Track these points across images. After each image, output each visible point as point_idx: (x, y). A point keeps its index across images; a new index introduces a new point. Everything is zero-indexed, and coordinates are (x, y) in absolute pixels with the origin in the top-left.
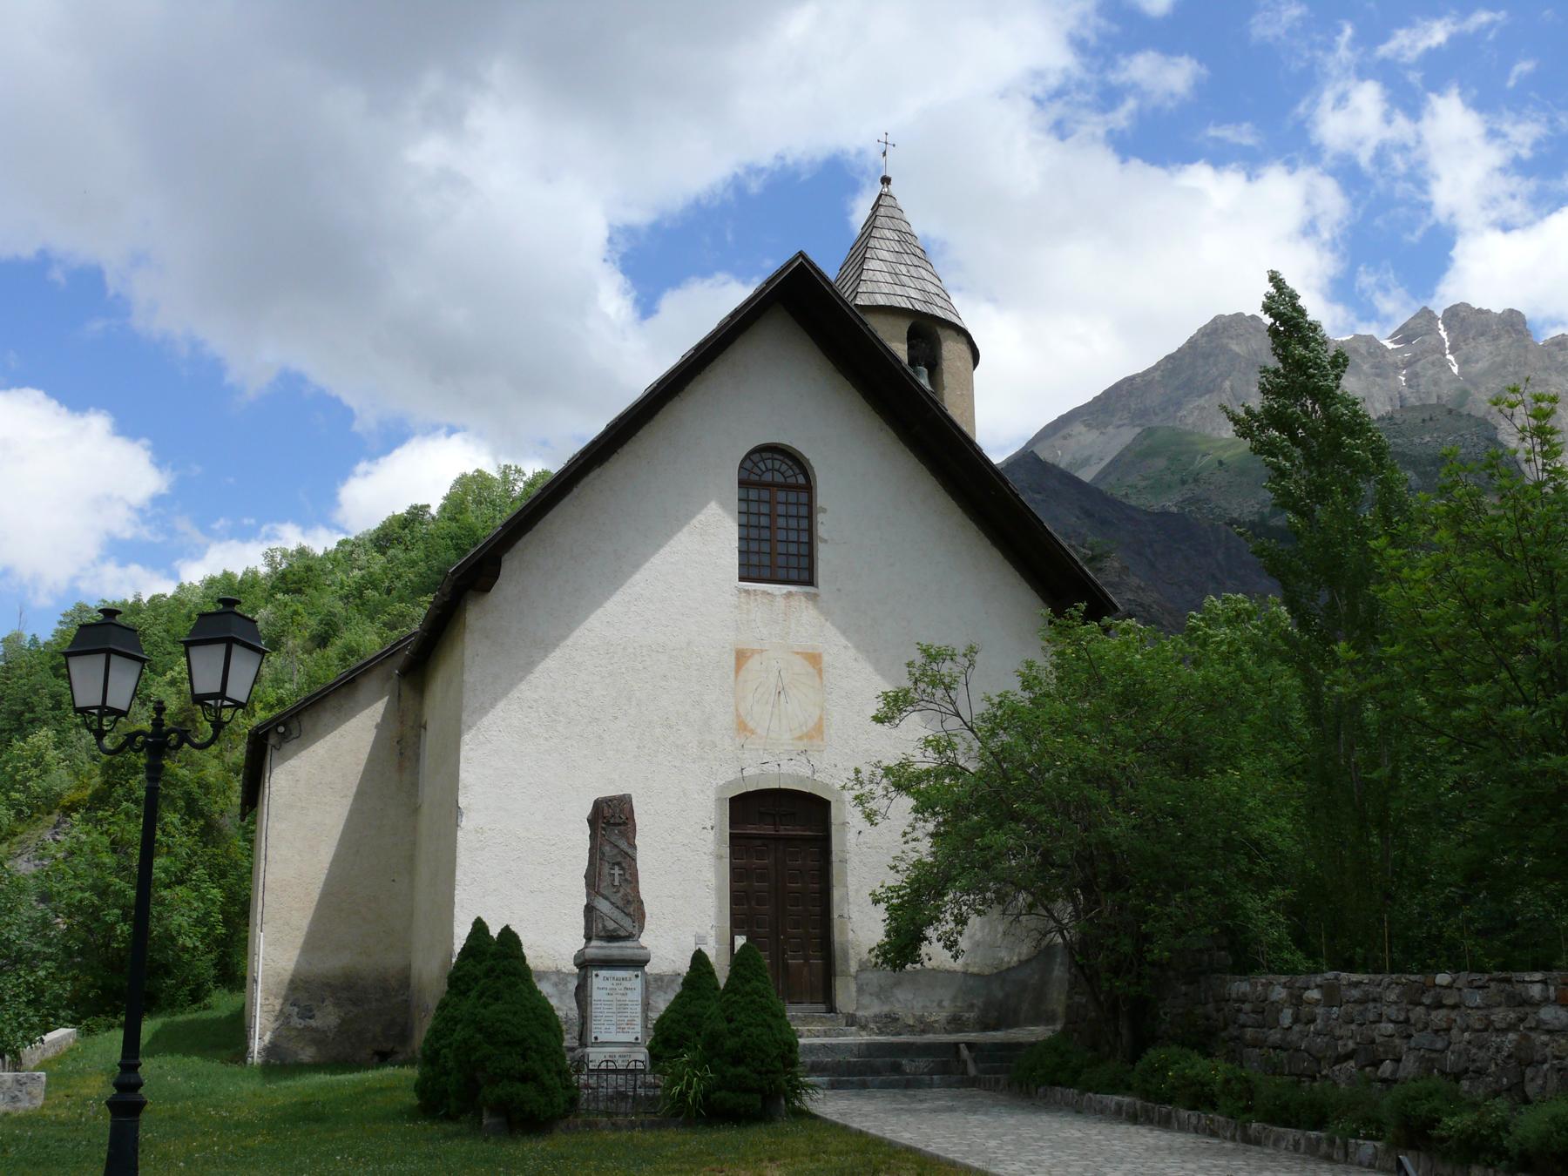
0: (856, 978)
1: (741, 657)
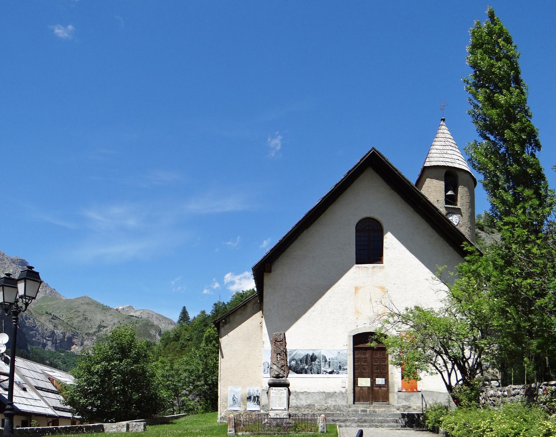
1: (357, 289)
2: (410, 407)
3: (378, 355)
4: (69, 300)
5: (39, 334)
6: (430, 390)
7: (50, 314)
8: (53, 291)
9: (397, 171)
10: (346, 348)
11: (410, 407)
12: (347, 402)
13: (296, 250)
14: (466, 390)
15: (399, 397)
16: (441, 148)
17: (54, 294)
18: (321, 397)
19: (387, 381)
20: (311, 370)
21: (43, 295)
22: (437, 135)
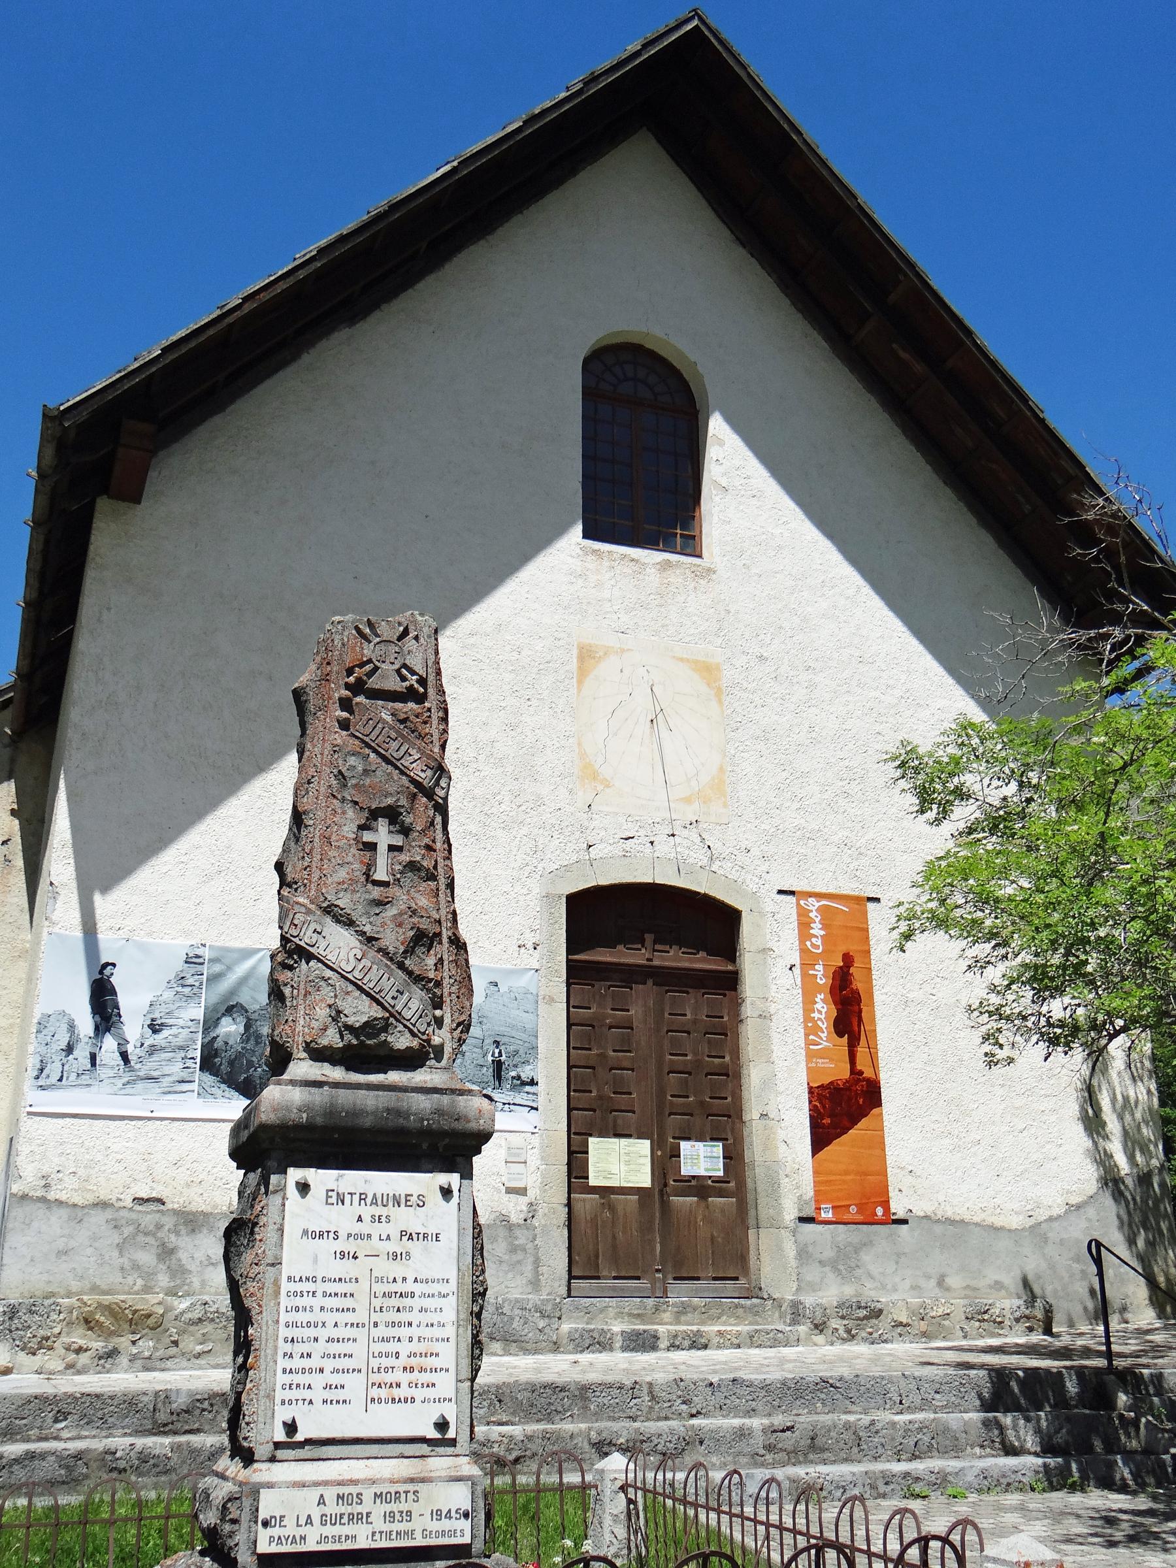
0: (794, 1232)
1: (587, 656)
2: (877, 1314)
3: (693, 1007)
9: (799, 133)
10: (533, 960)
11: (877, 1314)
12: (535, 1284)
13: (287, 413)
15: (803, 1254)
19: (734, 1158)
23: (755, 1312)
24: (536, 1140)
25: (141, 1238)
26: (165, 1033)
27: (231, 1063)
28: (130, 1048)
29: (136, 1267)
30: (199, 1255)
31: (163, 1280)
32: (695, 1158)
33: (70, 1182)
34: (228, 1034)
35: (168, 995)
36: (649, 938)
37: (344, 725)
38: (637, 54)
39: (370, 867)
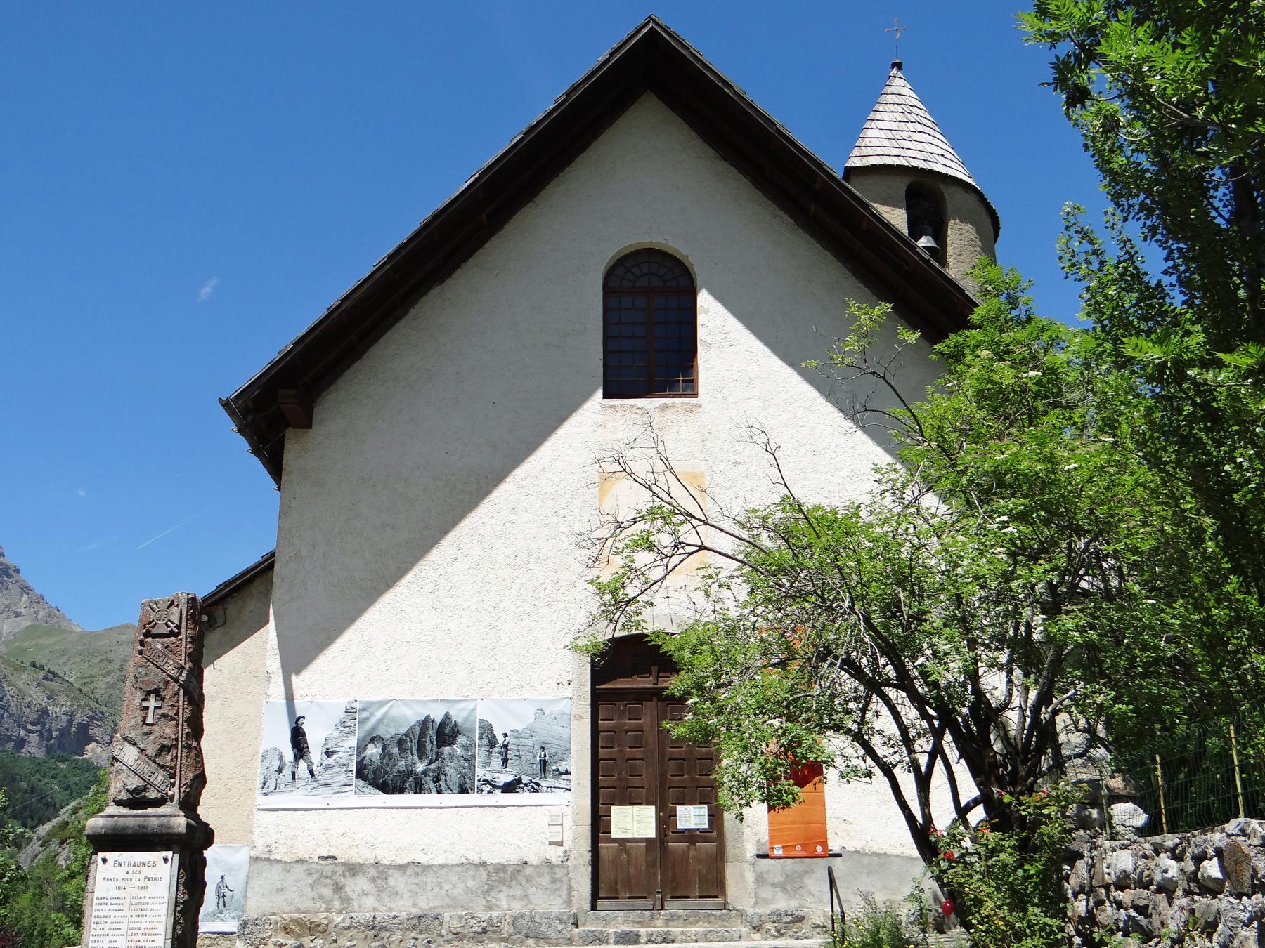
0: (753, 865)
4: (89, 633)
5: (11, 716)
6: (875, 849)
7: (42, 668)
8: (53, 613)
9: (730, 87)
10: (568, 691)
12: (569, 902)
13: (403, 353)
14: (993, 852)
15: (760, 880)
16: (894, 126)
17: (55, 620)
18: (471, 883)
20: (437, 780)
21: (28, 623)
22: (882, 99)
23: (723, 919)
24: (569, 810)
25: (323, 880)
26: (334, 757)
27: (374, 772)
28: (314, 767)
29: (321, 897)
30: (358, 890)
31: (337, 905)
32: (687, 817)
33: (283, 849)
34: (372, 755)
35: (336, 733)
36: (654, 669)
37: (141, 652)
38: (607, 61)
39: (145, 718)
